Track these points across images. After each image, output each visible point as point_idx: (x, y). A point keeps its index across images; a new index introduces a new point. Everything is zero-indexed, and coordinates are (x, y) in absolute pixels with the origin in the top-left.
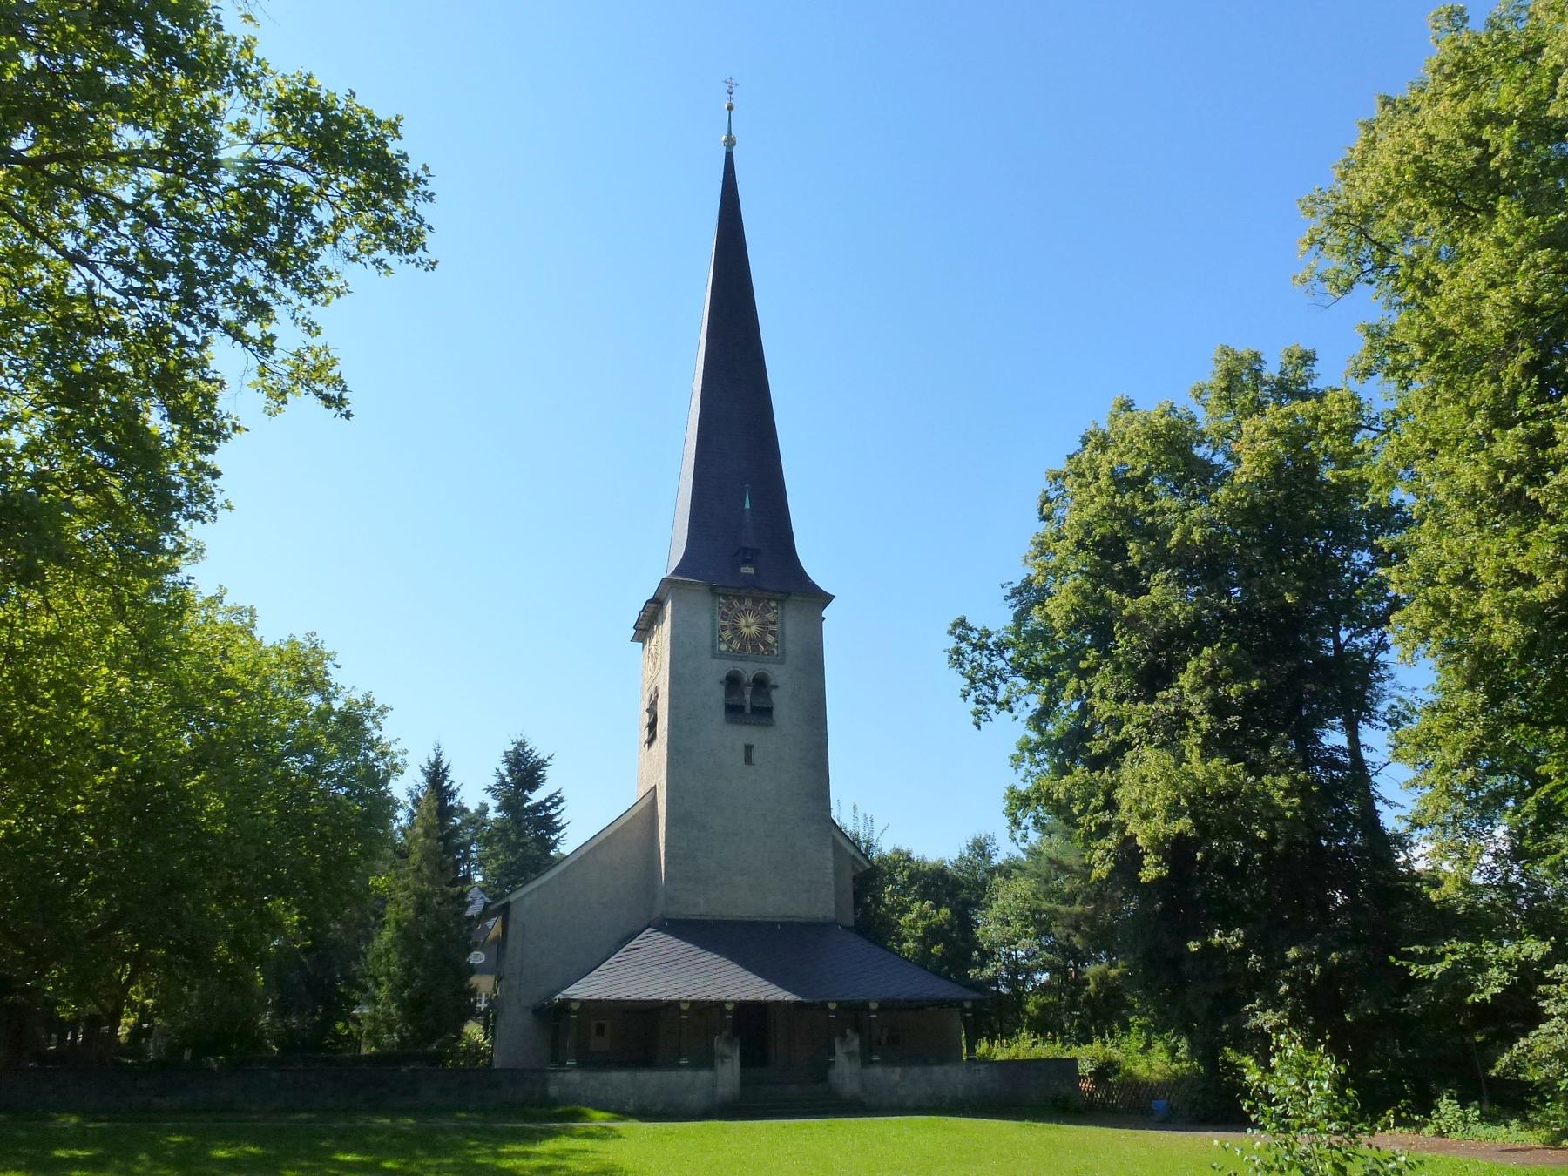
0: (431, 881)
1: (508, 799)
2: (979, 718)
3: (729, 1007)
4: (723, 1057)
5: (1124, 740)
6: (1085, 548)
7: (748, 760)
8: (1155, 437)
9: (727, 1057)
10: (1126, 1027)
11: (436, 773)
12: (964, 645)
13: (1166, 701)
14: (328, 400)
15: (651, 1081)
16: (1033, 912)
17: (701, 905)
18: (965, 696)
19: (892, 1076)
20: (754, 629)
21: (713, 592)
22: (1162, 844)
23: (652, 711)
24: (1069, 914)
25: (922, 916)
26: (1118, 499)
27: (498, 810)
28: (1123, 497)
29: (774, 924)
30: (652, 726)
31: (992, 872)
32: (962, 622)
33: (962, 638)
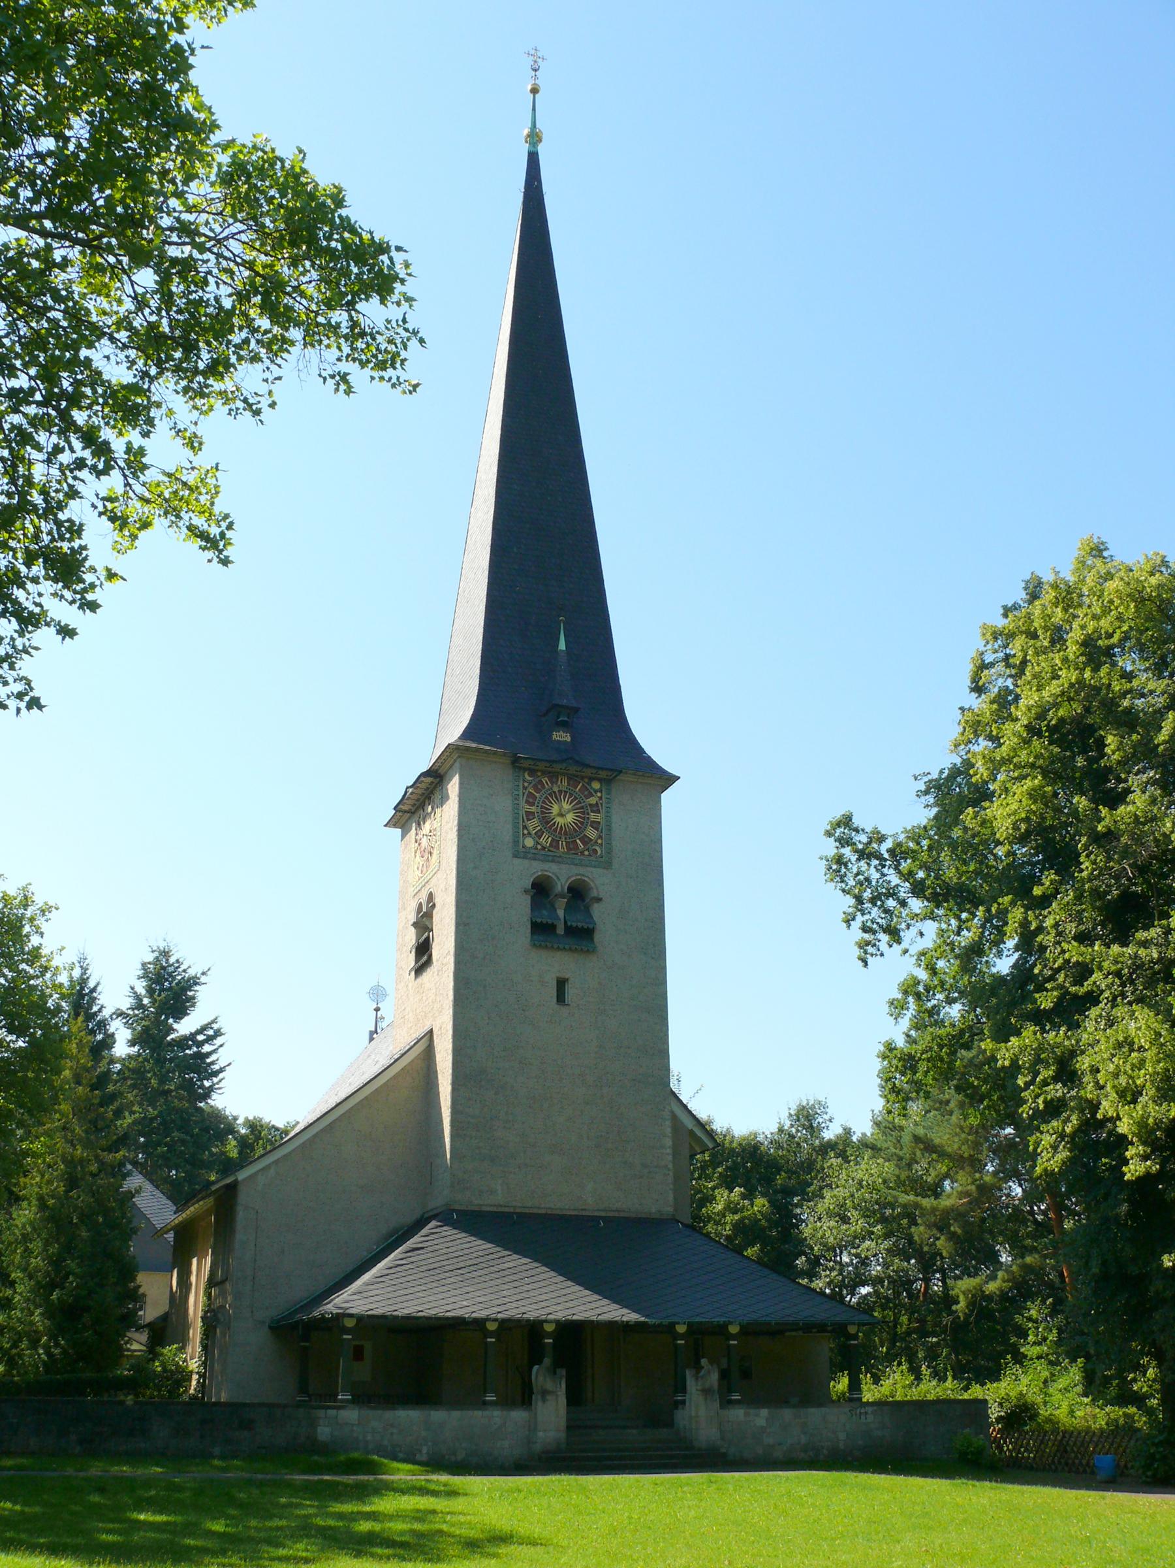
0: (87, 1145)
1: (146, 1030)
3: (549, 1328)
4: (545, 1393)
5: (1089, 994)
6: (1039, 734)
7: (561, 998)
8: (1139, 598)
9: (549, 1392)
10: (1019, 1359)
11: (81, 995)
12: (847, 851)
13: (1145, 944)
14: (211, 543)
15: (447, 1422)
17: (498, 1193)
18: (848, 922)
19: (755, 1421)
20: (570, 817)
21: (515, 762)
22: (1152, 1132)
25: (732, 1208)
28: (1096, 670)
29: (595, 1219)
30: (423, 950)
31: (827, 1148)
32: (846, 821)
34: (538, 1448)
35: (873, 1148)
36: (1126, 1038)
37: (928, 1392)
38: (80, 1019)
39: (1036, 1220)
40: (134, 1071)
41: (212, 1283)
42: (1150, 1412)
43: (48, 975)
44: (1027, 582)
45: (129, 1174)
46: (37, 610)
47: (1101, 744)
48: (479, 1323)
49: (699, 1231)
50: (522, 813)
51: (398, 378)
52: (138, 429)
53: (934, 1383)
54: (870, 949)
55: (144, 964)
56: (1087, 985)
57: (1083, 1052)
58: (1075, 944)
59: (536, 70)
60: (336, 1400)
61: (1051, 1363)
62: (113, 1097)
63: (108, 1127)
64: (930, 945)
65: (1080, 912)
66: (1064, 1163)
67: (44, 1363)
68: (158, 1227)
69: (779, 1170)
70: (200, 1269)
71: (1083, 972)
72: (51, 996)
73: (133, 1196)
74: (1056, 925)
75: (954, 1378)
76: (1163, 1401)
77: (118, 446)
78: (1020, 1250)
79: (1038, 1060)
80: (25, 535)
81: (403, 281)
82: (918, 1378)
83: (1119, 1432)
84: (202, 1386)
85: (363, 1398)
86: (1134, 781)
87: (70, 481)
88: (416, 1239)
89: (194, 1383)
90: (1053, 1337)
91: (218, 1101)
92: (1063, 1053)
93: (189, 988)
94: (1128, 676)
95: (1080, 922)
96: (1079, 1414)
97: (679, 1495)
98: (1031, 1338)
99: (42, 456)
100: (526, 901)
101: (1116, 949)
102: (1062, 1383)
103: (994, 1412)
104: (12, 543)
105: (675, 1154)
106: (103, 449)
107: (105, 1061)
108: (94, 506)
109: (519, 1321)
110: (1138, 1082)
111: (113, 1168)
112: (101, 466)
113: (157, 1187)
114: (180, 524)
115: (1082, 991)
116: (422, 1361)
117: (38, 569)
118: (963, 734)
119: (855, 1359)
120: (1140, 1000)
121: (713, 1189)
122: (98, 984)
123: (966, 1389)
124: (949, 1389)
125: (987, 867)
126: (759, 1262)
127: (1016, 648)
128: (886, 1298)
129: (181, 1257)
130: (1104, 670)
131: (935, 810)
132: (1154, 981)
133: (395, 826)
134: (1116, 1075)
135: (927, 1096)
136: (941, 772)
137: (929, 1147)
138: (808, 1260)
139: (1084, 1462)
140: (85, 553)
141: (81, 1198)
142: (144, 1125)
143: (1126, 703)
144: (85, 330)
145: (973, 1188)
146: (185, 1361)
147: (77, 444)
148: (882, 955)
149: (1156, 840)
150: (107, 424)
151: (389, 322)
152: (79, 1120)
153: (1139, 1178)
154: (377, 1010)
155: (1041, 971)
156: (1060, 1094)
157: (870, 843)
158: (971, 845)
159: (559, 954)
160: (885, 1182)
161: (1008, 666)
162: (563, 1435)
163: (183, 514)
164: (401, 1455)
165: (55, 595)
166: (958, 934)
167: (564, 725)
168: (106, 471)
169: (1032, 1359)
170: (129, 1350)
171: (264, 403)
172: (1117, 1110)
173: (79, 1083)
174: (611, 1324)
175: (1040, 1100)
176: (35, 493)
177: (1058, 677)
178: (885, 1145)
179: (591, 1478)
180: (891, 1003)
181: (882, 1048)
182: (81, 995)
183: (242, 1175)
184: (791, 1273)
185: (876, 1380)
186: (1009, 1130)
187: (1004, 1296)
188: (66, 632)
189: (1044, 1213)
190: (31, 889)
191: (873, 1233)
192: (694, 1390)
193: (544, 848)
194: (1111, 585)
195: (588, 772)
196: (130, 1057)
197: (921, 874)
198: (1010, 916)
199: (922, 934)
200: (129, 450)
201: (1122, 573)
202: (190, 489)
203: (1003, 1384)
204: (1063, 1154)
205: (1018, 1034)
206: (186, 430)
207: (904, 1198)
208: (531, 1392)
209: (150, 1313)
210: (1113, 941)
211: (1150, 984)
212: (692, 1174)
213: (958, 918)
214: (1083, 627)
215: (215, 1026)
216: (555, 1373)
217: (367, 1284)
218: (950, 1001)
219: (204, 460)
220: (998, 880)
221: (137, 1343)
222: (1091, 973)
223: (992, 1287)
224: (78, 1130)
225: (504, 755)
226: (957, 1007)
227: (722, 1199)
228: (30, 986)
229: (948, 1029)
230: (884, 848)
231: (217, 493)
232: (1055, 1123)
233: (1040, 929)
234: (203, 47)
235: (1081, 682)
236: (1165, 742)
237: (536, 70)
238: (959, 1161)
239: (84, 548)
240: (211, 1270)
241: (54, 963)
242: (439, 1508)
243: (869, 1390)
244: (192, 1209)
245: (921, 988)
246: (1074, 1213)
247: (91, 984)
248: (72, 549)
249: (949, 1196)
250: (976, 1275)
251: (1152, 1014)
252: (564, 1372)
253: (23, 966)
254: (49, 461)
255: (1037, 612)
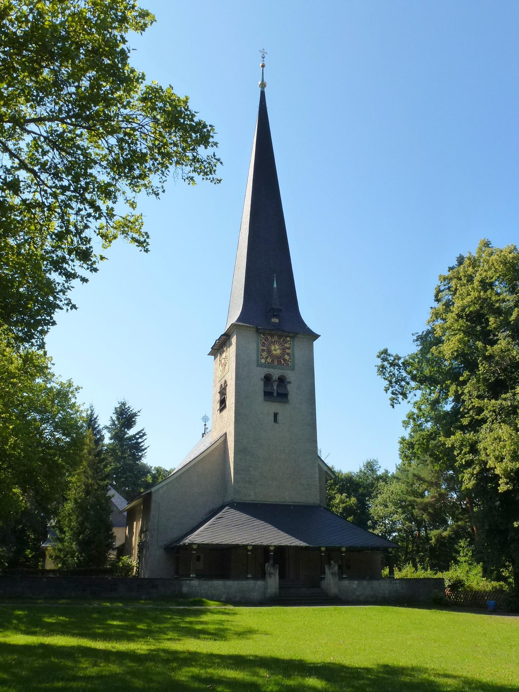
0: (93, 478)
1: (116, 433)
2: (393, 402)
3: (272, 548)
4: (270, 574)
5: (483, 419)
6: (462, 317)
7: (275, 420)
10: (457, 562)
11: (91, 420)
12: (386, 363)
13: (505, 399)
14: (140, 243)
15: (233, 585)
16: (402, 501)
17: (252, 495)
18: (386, 390)
19: (352, 585)
20: (278, 352)
21: (258, 331)
22: (509, 473)
23: (223, 392)
24: (421, 503)
26: (482, 293)
27: (111, 439)
28: (485, 291)
29: (290, 506)
30: (223, 403)
31: (378, 478)
32: (385, 352)
33: (384, 360)
34: (268, 595)
35: (397, 478)
36: (498, 436)
37: (421, 575)
38: (90, 430)
39: (462, 507)
40: (112, 450)
41: (142, 532)
42: (509, 584)
43: (78, 413)
44: (458, 258)
45: (110, 489)
46: (73, 272)
47: (487, 321)
48: (245, 547)
49: (329, 510)
50: (260, 350)
51: (213, 178)
52: (111, 201)
53: (423, 571)
54: (395, 401)
55: (116, 408)
56: (482, 416)
57: (480, 442)
58: (477, 399)
59: (263, 58)
60: (190, 577)
61: (469, 564)
62: (103, 460)
63: (101, 471)
64: (419, 400)
65: (478, 387)
66: (473, 485)
67: (77, 563)
68: (121, 510)
69: (360, 486)
70: (137, 526)
71: (480, 410)
72: (79, 421)
73: (111, 498)
74: (469, 392)
75: (431, 569)
76: (515, 579)
77: (103, 208)
78: (456, 519)
79: (462, 445)
80: (68, 242)
81: (212, 137)
82: (416, 569)
83: (498, 591)
84: (138, 572)
85: (200, 576)
86: (501, 335)
87: (85, 221)
88: (220, 514)
89: (135, 570)
90: (470, 554)
91: (144, 461)
92: (472, 442)
93: (133, 417)
94: (498, 294)
95: (479, 391)
96: (481, 584)
97: (323, 614)
98: (461, 554)
99: (74, 212)
100: (261, 384)
101: (493, 401)
102: (474, 572)
103: (447, 583)
104: (63, 246)
105: (320, 480)
106: (97, 209)
107: (100, 446)
108: (95, 231)
109: (260, 546)
110: (503, 454)
111: (103, 487)
112: (97, 216)
113: (120, 494)
114: (128, 237)
115: (480, 418)
116: (224, 563)
117: (73, 256)
118: (431, 318)
119: (392, 562)
120: (504, 422)
121: (335, 494)
122: (97, 416)
123: (435, 574)
124: (429, 574)
125: (442, 369)
126: (353, 523)
127: (453, 283)
128: (403, 537)
129: (129, 522)
130: (489, 292)
131: (420, 347)
132: (509, 414)
133: (212, 355)
134: (494, 451)
135: (418, 458)
136: (423, 332)
137: (419, 478)
138: (372, 522)
139: (483, 603)
140: (91, 249)
141: (91, 499)
142: (116, 470)
143: (497, 305)
144: (89, 162)
145: (437, 494)
146: (131, 562)
147: (87, 207)
148: (400, 403)
149: (510, 359)
150: (99, 199)
151: (208, 156)
152: (90, 469)
153: (505, 492)
154: (205, 425)
155: (463, 410)
156: (471, 458)
157: (394, 360)
158: (435, 360)
159: (275, 403)
160: (402, 492)
161: (450, 290)
162: (277, 590)
163: (129, 233)
164: (215, 599)
165: (80, 266)
166: (430, 395)
167: (275, 316)
168: (99, 218)
169: (462, 562)
170: (109, 558)
171: (160, 191)
172: (495, 465)
173: (90, 454)
174: (296, 547)
175: (463, 460)
176: (71, 226)
177: (470, 295)
178: (401, 478)
179: (288, 608)
180: (404, 422)
181: (400, 440)
182: (91, 420)
183: (153, 489)
184: (365, 527)
185: (400, 570)
186: (451, 472)
187: (450, 536)
188: (84, 280)
189: (466, 505)
190: (72, 380)
191: (397, 512)
192: (328, 573)
193: (268, 363)
194: (494, 257)
195: (285, 334)
196: (110, 444)
197: (415, 372)
198: (450, 388)
199: (415, 395)
200: (108, 208)
201: (498, 253)
202: (132, 223)
203: (450, 572)
204: (473, 482)
205: (454, 434)
206: (130, 200)
207: (412, 498)
208: (265, 574)
209: (118, 543)
210: (492, 398)
211: (508, 415)
212: (326, 488)
213: (430, 389)
214: (481, 275)
215: (143, 432)
216: (274, 566)
217: (201, 531)
218: (427, 421)
219: (137, 212)
220: (446, 374)
221: (112, 555)
222: (483, 411)
223: (445, 534)
224: (90, 473)
225: (253, 327)
226: (430, 423)
227: (338, 498)
228: (71, 418)
229: (427, 432)
230: (400, 362)
231: (142, 225)
232: (469, 470)
233: (463, 393)
234: (133, 49)
235: (479, 297)
236: (513, 320)
237: (263, 58)
238: (431, 484)
239: (91, 247)
240: (141, 527)
241: (80, 409)
242: (230, 619)
243: (397, 574)
244: (134, 503)
245: (415, 416)
246: (478, 505)
247: (95, 416)
248: (86, 248)
249: (427, 498)
250: (438, 529)
251: (508, 427)
252: (278, 566)
253: (68, 410)
254: (77, 214)
255: (462, 270)
